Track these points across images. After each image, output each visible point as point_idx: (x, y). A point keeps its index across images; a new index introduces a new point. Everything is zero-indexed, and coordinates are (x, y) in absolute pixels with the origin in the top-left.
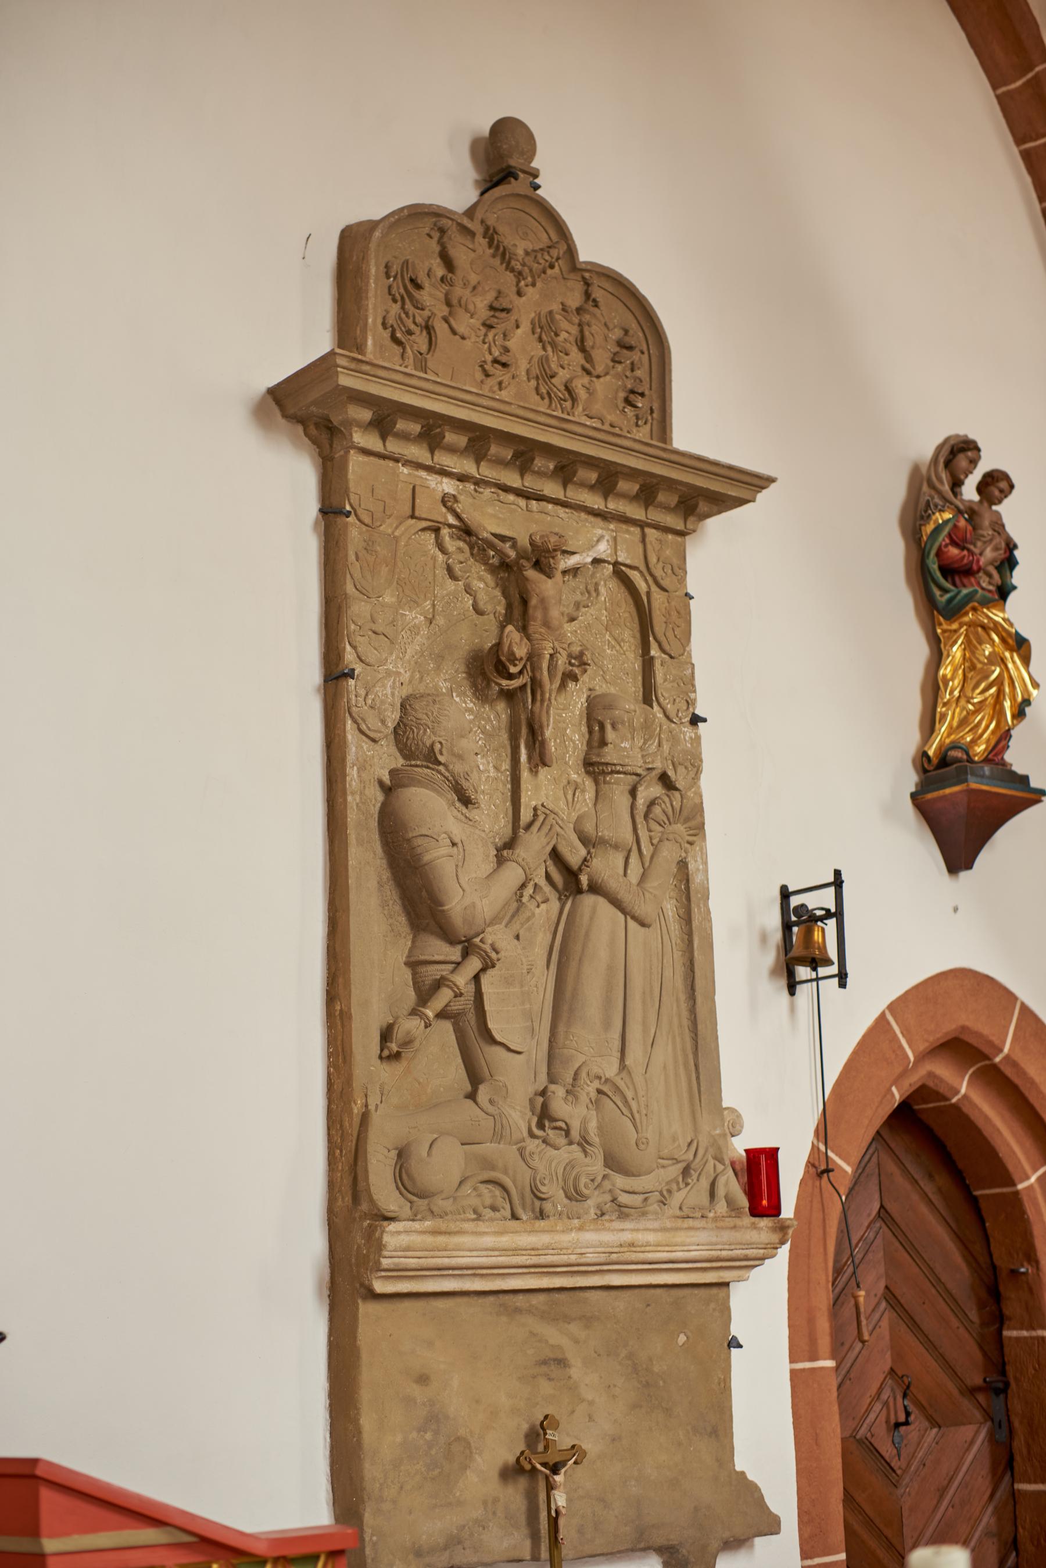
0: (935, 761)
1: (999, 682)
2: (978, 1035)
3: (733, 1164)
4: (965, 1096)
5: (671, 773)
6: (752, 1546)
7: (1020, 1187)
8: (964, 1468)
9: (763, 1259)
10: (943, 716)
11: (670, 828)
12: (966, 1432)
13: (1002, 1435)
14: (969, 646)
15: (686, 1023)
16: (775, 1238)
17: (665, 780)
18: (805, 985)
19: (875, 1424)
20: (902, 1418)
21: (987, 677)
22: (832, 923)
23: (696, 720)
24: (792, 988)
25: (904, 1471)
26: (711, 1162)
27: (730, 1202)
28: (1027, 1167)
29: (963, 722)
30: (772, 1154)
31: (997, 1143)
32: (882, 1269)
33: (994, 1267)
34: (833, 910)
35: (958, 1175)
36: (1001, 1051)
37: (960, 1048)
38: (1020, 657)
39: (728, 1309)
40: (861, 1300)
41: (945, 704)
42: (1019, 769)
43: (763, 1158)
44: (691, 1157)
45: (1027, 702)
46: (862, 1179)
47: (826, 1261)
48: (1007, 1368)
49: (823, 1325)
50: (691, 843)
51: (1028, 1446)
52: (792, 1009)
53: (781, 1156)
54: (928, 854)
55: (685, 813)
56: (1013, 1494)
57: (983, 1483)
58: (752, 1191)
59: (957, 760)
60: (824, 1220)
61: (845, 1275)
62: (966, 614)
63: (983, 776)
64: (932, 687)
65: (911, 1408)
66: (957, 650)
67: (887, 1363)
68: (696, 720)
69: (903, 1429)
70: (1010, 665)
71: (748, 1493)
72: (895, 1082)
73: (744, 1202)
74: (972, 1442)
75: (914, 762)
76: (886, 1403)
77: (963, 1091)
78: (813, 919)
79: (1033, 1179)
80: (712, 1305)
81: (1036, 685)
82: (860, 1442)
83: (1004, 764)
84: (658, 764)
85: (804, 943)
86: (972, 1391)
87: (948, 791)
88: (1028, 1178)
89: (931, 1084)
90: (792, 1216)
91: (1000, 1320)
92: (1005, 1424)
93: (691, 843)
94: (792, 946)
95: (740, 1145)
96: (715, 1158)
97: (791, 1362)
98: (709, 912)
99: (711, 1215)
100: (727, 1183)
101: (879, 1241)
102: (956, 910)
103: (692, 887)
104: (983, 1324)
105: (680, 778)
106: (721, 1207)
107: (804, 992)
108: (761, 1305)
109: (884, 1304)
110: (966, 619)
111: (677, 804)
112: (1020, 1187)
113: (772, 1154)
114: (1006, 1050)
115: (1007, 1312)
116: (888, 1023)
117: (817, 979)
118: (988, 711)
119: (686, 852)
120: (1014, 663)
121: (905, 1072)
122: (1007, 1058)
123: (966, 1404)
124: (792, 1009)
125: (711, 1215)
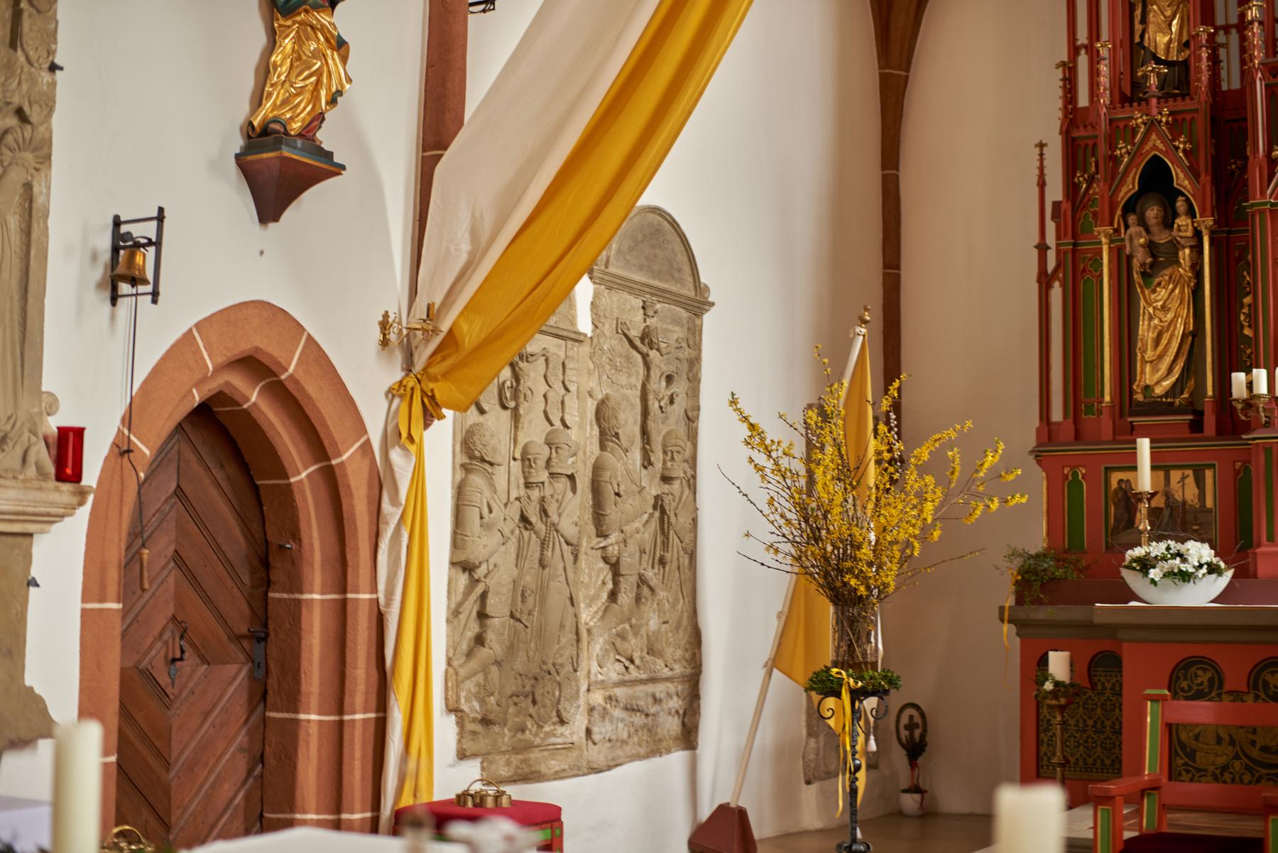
0: (258, 130)
1: (318, 73)
2: (270, 356)
3: (46, 439)
4: (254, 404)
5: (26, 109)
6: (35, 747)
7: (292, 480)
8: (226, 698)
9: (62, 516)
10: (270, 94)
11: (18, 155)
12: (232, 669)
13: (260, 674)
14: (299, 40)
15: (17, 318)
16: (74, 500)
17: (20, 113)
18: (126, 299)
19: (156, 659)
20: (178, 655)
21: (309, 68)
22: (152, 250)
23: (53, 68)
24: (114, 299)
25: (177, 696)
26: (27, 434)
27: (39, 467)
28: (300, 466)
29: (285, 102)
30: (79, 433)
31: (281, 451)
32: (173, 537)
33: (267, 542)
34: (154, 240)
35: (244, 467)
36: (286, 370)
37: (253, 365)
38: (339, 55)
39: (30, 555)
40: (145, 557)
41: (272, 85)
42: (326, 146)
43: (71, 435)
44: (8, 427)
45: (340, 93)
46: (164, 462)
47: (120, 524)
48: (270, 622)
49: (113, 575)
50: (37, 170)
51: (279, 684)
52: (113, 317)
53: (86, 434)
54: (244, 204)
55: (34, 144)
56: (264, 720)
57: (240, 711)
58: (60, 463)
59: (277, 132)
60: (122, 491)
61: (138, 535)
62: (299, 14)
63: (295, 148)
64: (265, 70)
65: (186, 647)
66: (288, 43)
67: (171, 610)
68: (53, 68)
69: (178, 663)
70: (330, 62)
71: (35, 703)
72: (196, 385)
73: (51, 469)
74: (235, 678)
75: (241, 129)
76: (166, 643)
77: (253, 399)
78: (137, 245)
79: (303, 475)
80: (17, 551)
81: (349, 80)
82: (142, 672)
83: (313, 139)
84: (16, 100)
85: (127, 265)
86: (239, 638)
87: (265, 156)
88: (299, 473)
89: (227, 391)
90: (94, 485)
91: (268, 584)
92: (263, 665)
93: (37, 170)
94: (118, 262)
95: (53, 424)
96: (30, 431)
97: (84, 600)
98: (47, 228)
99: (21, 477)
100: (38, 452)
101: (173, 513)
102: (262, 253)
103: (35, 206)
104: (253, 587)
105: (34, 114)
106: (31, 471)
107: (124, 305)
108: (61, 558)
109: (172, 564)
110: (298, 18)
111: (27, 134)
112: (292, 480)
113: (79, 433)
114: (291, 370)
115: (272, 578)
116: (194, 338)
117: (137, 295)
118: (307, 95)
119: (32, 176)
120: (333, 59)
121: (204, 379)
122: (291, 376)
123: (232, 648)
124: (113, 317)
125: (21, 477)
